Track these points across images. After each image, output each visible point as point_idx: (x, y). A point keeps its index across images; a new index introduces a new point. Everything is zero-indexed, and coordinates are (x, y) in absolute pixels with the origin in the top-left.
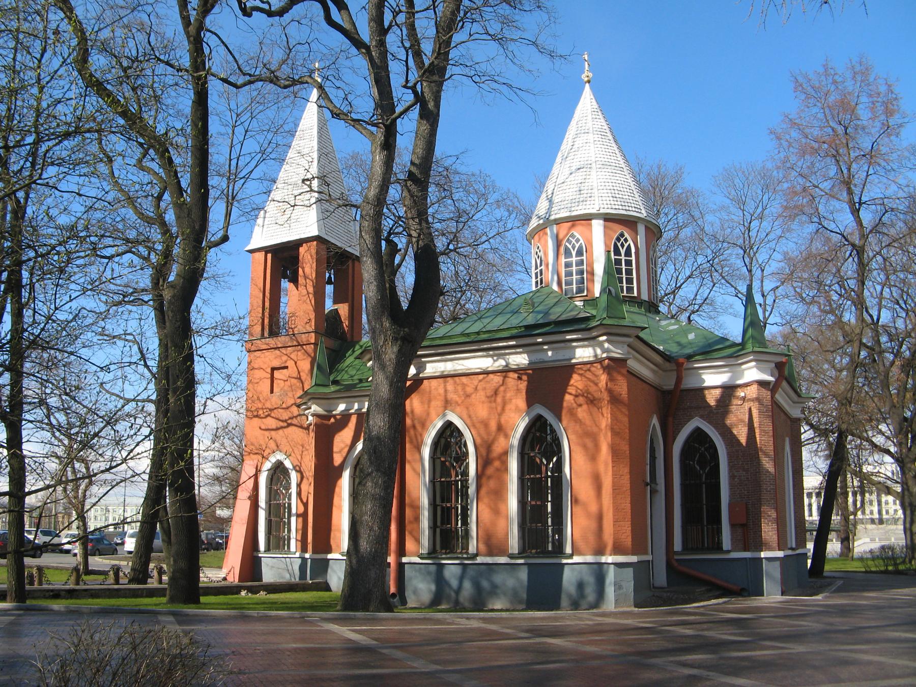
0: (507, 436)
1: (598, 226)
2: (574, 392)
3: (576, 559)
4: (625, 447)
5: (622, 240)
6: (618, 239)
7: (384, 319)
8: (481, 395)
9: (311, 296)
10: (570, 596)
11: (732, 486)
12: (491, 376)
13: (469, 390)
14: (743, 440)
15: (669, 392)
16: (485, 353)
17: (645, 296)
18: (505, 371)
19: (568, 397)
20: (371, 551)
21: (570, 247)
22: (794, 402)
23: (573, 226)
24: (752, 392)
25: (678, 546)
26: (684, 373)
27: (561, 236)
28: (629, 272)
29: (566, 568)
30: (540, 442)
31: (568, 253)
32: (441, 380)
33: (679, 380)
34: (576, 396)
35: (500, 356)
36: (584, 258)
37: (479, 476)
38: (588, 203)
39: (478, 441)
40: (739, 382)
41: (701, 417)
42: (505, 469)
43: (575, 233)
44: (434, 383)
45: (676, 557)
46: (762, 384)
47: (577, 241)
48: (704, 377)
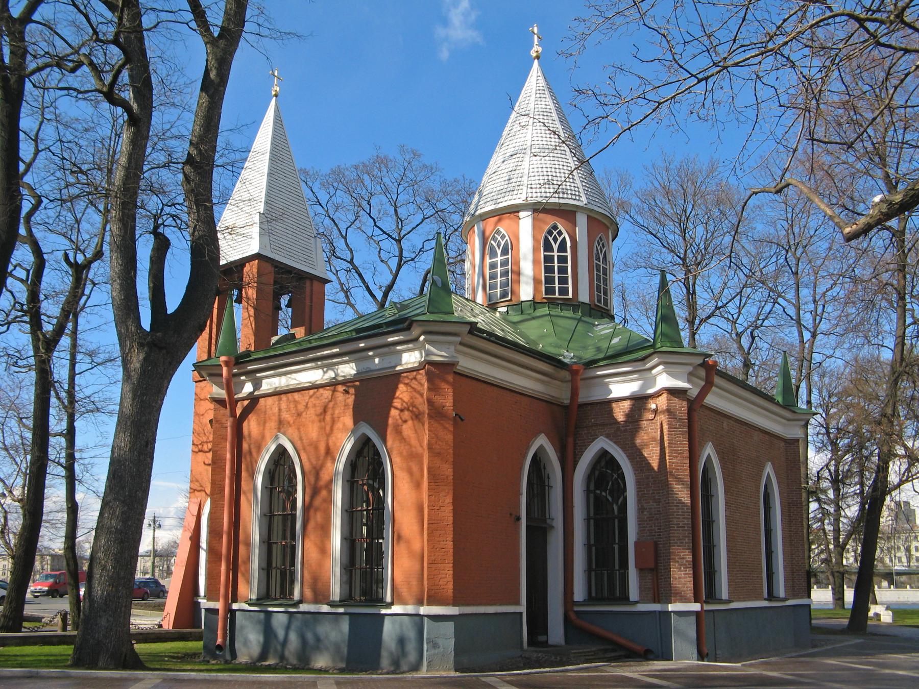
0: (334, 460)
1: (526, 221)
2: (399, 406)
3: (396, 609)
4: (447, 470)
5: (555, 233)
6: (550, 233)
7: (129, 323)
8: (311, 414)
9: (252, 319)
10: (391, 653)
11: (641, 522)
12: (321, 390)
13: (301, 407)
14: (655, 464)
15: (566, 408)
16: (313, 364)
17: (584, 297)
18: (333, 384)
19: (394, 412)
20: (102, 594)
21: (495, 245)
22: (789, 420)
23: (500, 220)
24: (662, 402)
25: (579, 594)
26: (580, 384)
27: (487, 233)
28: (563, 270)
29: (387, 621)
30: (367, 467)
31: (493, 254)
32: (276, 398)
33: (574, 393)
34: (402, 410)
35: (330, 367)
36: (510, 256)
37: (306, 509)
38: (516, 192)
39: (307, 467)
40: (651, 391)
41: (608, 436)
42: (329, 501)
43: (501, 230)
44: (270, 400)
45: (576, 609)
46: (673, 392)
47: (503, 237)
48: (611, 387)
